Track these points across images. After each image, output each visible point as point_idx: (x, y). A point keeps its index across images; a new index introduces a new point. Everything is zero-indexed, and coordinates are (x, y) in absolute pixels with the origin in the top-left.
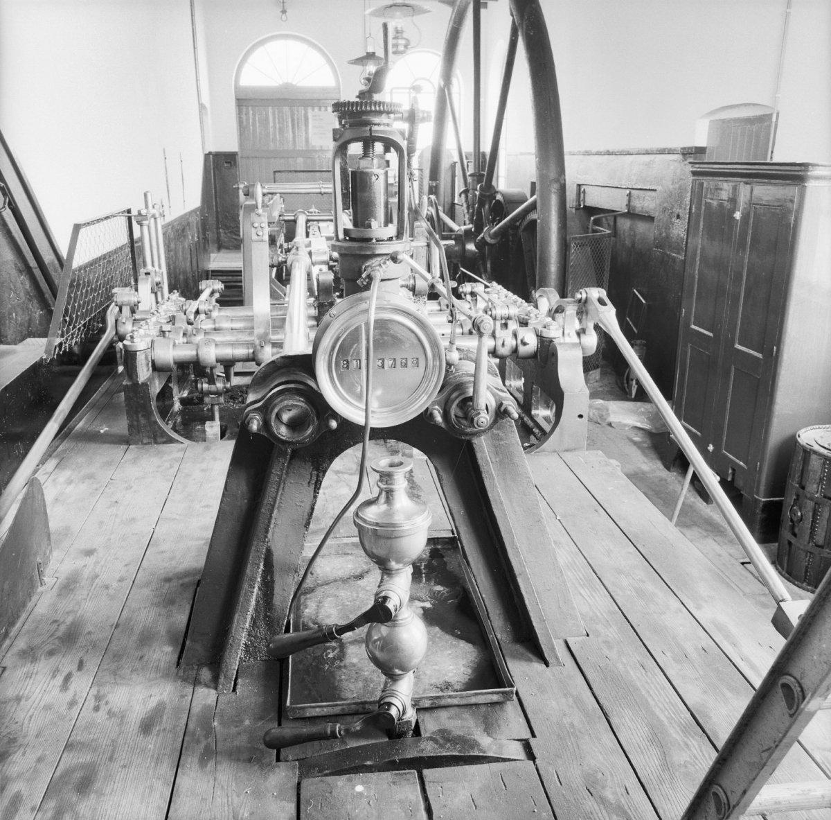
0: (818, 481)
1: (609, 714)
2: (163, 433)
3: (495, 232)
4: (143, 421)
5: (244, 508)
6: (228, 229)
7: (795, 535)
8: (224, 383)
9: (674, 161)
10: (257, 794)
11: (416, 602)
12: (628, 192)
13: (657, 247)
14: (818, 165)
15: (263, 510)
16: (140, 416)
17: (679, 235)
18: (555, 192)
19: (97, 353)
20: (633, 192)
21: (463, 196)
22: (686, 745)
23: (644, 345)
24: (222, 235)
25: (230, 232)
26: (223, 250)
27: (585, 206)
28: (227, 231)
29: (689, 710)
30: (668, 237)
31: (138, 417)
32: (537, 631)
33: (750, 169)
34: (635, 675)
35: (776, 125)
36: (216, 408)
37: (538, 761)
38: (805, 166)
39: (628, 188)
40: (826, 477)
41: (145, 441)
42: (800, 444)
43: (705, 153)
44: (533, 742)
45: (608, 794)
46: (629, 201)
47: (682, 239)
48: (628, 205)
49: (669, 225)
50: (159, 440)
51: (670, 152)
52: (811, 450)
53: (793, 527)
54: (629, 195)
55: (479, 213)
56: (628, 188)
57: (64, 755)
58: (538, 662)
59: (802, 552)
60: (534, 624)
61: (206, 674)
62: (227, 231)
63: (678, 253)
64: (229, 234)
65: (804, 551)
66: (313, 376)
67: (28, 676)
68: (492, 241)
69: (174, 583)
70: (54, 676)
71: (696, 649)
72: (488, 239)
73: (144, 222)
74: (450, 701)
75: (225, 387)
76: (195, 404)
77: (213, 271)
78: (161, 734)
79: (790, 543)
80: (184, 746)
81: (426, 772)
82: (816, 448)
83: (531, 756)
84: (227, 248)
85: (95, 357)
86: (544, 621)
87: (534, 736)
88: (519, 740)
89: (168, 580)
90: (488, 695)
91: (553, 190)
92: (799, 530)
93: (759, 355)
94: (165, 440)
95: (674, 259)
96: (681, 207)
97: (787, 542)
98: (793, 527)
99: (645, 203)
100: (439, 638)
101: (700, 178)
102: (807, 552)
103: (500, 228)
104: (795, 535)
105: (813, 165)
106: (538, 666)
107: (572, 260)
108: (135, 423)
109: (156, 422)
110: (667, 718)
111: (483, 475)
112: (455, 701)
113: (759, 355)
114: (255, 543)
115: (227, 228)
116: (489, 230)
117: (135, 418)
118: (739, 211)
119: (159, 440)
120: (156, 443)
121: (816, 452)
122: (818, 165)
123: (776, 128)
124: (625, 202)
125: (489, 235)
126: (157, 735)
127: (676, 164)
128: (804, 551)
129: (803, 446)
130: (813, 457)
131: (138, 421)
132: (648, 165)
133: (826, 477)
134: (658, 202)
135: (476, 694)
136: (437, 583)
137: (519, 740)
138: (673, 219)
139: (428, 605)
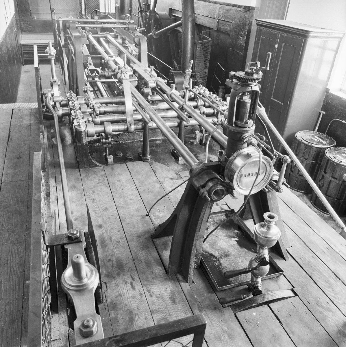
0: (303, 153)
1: (312, 277)
2: (93, 163)
3: (158, 33)
4: (85, 159)
5: (187, 218)
6: (25, 22)
7: (292, 171)
8: (112, 139)
9: (241, 11)
10: (225, 321)
11: (232, 238)
12: (218, 21)
13: (230, 47)
14: (313, 32)
15: (199, 221)
16: (84, 157)
17: (241, 44)
18: (190, 22)
19: (57, 129)
20: (220, 21)
21: (140, 13)
22: (337, 285)
23: (224, 88)
24: (22, 25)
25: (26, 24)
26: (23, 33)
27: (196, 24)
28: (24, 23)
29: (333, 272)
30: (236, 43)
31: (83, 158)
32: (282, 250)
33: (284, 28)
34: (312, 260)
35: (289, 3)
36: (108, 149)
37: (299, 296)
38: (307, 32)
39: (218, 19)
40: (306, 152)
41: (85, 167)
42: (297, 139)
43: (255, 10)
44: (294, 289)
45: (323, 305)
46: (218, 25)
47: (243, 46)
48: (217, 27)
49: (237, 39)
50: (91, 166)
51: (239, 6)
52: (301, 142)
53: (291, 169)
54: (218, 22)
55: (149, 24)
56: (218, 19)
57: (153, 315)
58: (282, 259)
59: (294, 177)
60: (281, 247)
61: (180, 277)
62: (24, 23)
63: (241, 51)
64: (25, 25)
65: (295, 177)
66: (233, 183)
67: (117, 285)
68: (156, 37)
69: (143, 238)
70: (126, 284)
71: (325, 248)
72: (154, 36)
73: (53, 58)
74: (265, 278)
75: (112, 140)
76: (92, 143)
77: (23, 45)
78: (180, 303)
79: (290, 174)
80: (191, 306)
81: (270, 305)
82: (303, 141)
83: (296, 295)
84: (25, 31)
85: (58, 131)
86: (284, 246)
87: (294, 287)
88: (290, 289)
89: (139, 237)
90: (276, 274)
91: (190, 21)
92: (294, 170)
93: (282, 104)
94: (94, 165)
95: (239, 54)
96: (243, 32)
97: (289, 174)
98: (291, 169)
99: (227, 27)
100: (248, 253)
101: (260, 27)
102: (296, 177)
103: (160, 32)
104: (292, 171)
105: (311, 32)
106: (283, 261)
107: (198, 52)
108: (82, 160)
109: (90, 159)
110: (328, 276)
111: (268, 201)
112: (267, 278)
113: (282, 104)
114: (196, 232)
115: (25, 21)
116: (155, 32)
117: (82, 158)
118: (277, 44)
119: (91, 166)
120: (90, 167)
121: (303, 143)
122: (313, 32)
123: (289, 5)
124: (216, 26)
125: (155, 34)
126: (179, 303)
127: (242, 13)
128: (295, 177)
129: (298, 140)
130: (302, 145)
131: (83, 159)
132: (228, 10)
133: (306, 152)
134: (232, 28)
135: (273, 275)
136: (235, 229)
137: (290, 289)
138: (239, 36)
139: (237, 239)
